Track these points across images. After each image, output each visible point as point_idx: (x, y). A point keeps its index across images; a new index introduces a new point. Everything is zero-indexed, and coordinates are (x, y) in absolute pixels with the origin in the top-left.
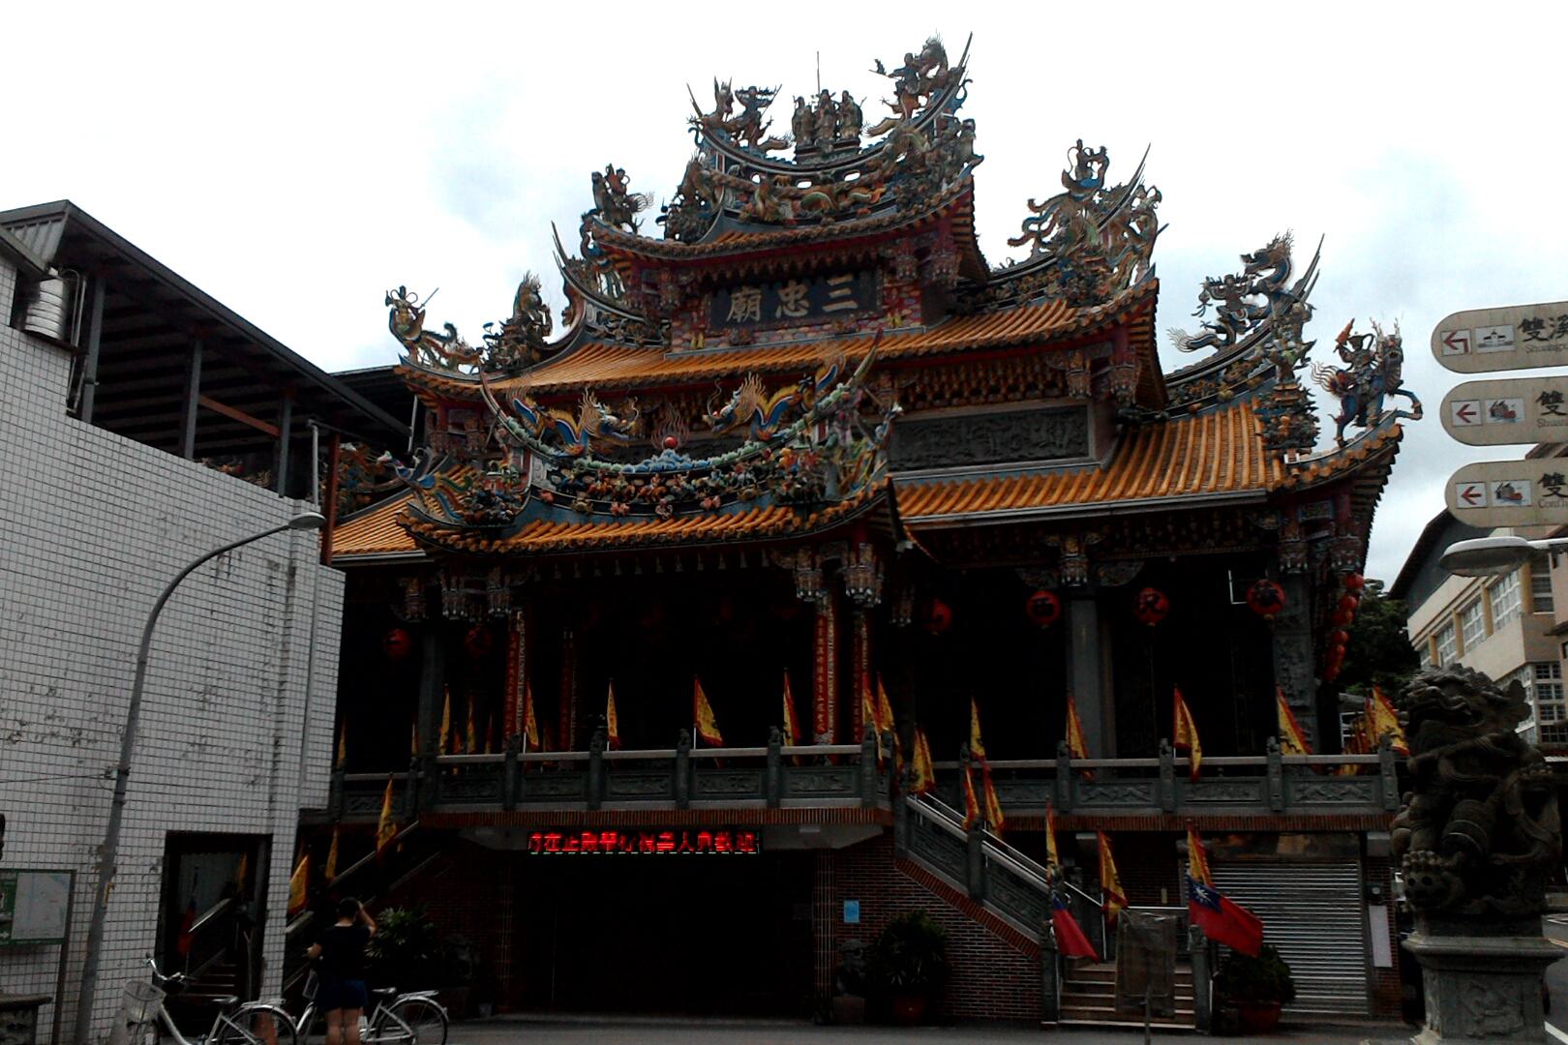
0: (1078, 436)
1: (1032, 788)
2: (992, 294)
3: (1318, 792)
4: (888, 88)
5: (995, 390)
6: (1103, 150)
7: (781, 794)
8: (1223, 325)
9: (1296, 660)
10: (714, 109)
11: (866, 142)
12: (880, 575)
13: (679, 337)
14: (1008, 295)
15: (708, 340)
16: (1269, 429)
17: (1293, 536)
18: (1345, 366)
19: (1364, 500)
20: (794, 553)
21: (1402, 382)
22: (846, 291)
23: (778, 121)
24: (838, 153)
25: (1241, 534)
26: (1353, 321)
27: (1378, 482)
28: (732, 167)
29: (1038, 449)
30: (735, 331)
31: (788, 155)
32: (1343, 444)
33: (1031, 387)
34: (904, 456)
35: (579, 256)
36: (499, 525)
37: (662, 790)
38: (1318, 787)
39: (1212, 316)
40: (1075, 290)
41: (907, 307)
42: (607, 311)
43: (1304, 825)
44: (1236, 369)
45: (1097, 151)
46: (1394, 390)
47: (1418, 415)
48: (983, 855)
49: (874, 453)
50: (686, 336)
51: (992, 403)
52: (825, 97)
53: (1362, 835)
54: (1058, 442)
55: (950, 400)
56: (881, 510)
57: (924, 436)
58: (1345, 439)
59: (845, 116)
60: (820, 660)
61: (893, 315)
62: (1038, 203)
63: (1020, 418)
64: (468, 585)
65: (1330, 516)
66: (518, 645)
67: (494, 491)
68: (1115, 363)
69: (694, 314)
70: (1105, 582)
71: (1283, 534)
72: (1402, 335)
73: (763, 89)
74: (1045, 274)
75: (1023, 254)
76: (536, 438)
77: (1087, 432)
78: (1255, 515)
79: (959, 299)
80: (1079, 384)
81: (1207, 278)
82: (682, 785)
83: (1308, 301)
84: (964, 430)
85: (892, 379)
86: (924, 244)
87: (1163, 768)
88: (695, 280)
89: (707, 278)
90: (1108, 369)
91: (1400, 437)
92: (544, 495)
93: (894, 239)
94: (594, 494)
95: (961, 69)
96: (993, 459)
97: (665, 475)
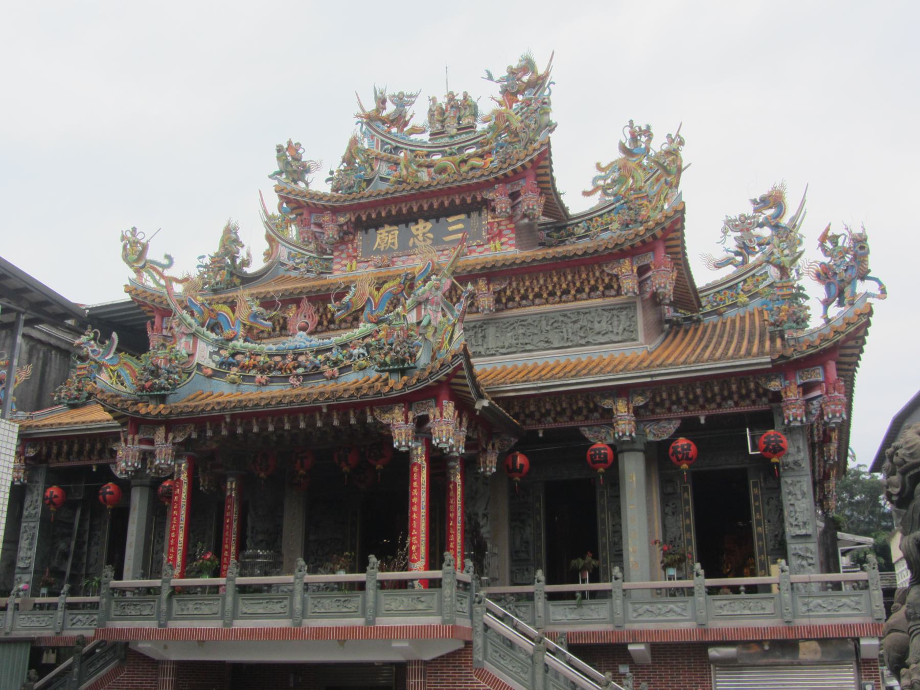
0: (630, 326)
1: (593, 607)
2: (571, 231)
3: (820, 605)
4: (495, 90)
5: (566, 292)
6: (648, 127)
7: (376, 614)
8: (739, 250)
9: (800, 497)
10: (374, 108)
11: (480, 127)
12: (463, 429)
13: (339, 263)
14: (583, 231)
15: (360, 265)
16: (772, 315)
17: (793, 394)
18: (827, 260)
19: (846, 367)
20: (390, 410)
21: (869, 271)
22: (461, 226)
23: (418, 115)
24: (460, 134)
25: (753, 395)
26: (830, 225)
27: (856, 351)
28: (386, 147)
29: (600, 336)
30: (379, 257)
31: (426, 137)
32: (828, 321)
33: (594, 289)
34: (500, 344)
35: (277, 213)
36: (163, 392)
37: (282, 611)
38: (819, 601)
39: (732, 245)
40: (626, 217)
41: (505, 236)
42: (295, 251)
43: (809, 632)
44: (749, 282)
45: (644, 128)
46: (864, 276)
47: (883, 296)
48: (546, 665)
49: (454, 325)
50: (344, 262)
51: (565, 302)
52: (451, 97)
53: (857, 640)
54: (615, 331)
55: (533, 301)
56: (460, 373)
57: (514, 328)
58: (830, 317)
59: (465, 109)
60: (415, 500)
61: (494, 242)
62: (603, 165)
63: (586, 313)
64: (141, 442)
65: (821, 379)
66: (181, 491)
67: (162, 366)
68: (655, 267)
69: (350, 246)
70: (651, 438)
71: (786, 393)
72: (868, 233)
73: (409, 93)
74: (610, 215)
75: (594, 201)
76: (203, 327)
77: (637, 323)
78: (763, 380)
79: (548, 235)
80: (629, 284)
81: (726, 216)
82: (298, 606)
83: (799, 232)
84: (544, 322)
85: (488, 284)
86: (516, 189)
87: (696, 588)
88: (350, 219)
89: (359, 218)
90: (650, 273)
91: (870, 313)
92: (205, 370)
93: (493, 185)
94: (244, 368)
95: (547, 74)
96: (566, 345)
97: (297, 354)
